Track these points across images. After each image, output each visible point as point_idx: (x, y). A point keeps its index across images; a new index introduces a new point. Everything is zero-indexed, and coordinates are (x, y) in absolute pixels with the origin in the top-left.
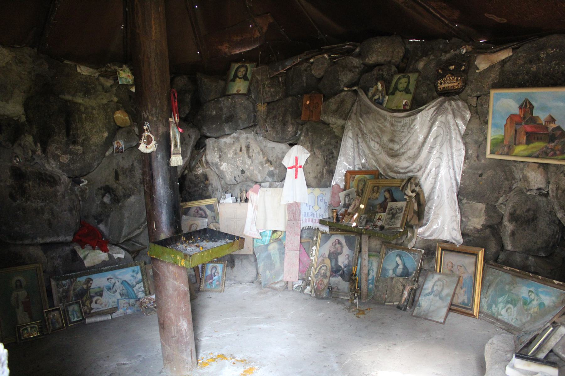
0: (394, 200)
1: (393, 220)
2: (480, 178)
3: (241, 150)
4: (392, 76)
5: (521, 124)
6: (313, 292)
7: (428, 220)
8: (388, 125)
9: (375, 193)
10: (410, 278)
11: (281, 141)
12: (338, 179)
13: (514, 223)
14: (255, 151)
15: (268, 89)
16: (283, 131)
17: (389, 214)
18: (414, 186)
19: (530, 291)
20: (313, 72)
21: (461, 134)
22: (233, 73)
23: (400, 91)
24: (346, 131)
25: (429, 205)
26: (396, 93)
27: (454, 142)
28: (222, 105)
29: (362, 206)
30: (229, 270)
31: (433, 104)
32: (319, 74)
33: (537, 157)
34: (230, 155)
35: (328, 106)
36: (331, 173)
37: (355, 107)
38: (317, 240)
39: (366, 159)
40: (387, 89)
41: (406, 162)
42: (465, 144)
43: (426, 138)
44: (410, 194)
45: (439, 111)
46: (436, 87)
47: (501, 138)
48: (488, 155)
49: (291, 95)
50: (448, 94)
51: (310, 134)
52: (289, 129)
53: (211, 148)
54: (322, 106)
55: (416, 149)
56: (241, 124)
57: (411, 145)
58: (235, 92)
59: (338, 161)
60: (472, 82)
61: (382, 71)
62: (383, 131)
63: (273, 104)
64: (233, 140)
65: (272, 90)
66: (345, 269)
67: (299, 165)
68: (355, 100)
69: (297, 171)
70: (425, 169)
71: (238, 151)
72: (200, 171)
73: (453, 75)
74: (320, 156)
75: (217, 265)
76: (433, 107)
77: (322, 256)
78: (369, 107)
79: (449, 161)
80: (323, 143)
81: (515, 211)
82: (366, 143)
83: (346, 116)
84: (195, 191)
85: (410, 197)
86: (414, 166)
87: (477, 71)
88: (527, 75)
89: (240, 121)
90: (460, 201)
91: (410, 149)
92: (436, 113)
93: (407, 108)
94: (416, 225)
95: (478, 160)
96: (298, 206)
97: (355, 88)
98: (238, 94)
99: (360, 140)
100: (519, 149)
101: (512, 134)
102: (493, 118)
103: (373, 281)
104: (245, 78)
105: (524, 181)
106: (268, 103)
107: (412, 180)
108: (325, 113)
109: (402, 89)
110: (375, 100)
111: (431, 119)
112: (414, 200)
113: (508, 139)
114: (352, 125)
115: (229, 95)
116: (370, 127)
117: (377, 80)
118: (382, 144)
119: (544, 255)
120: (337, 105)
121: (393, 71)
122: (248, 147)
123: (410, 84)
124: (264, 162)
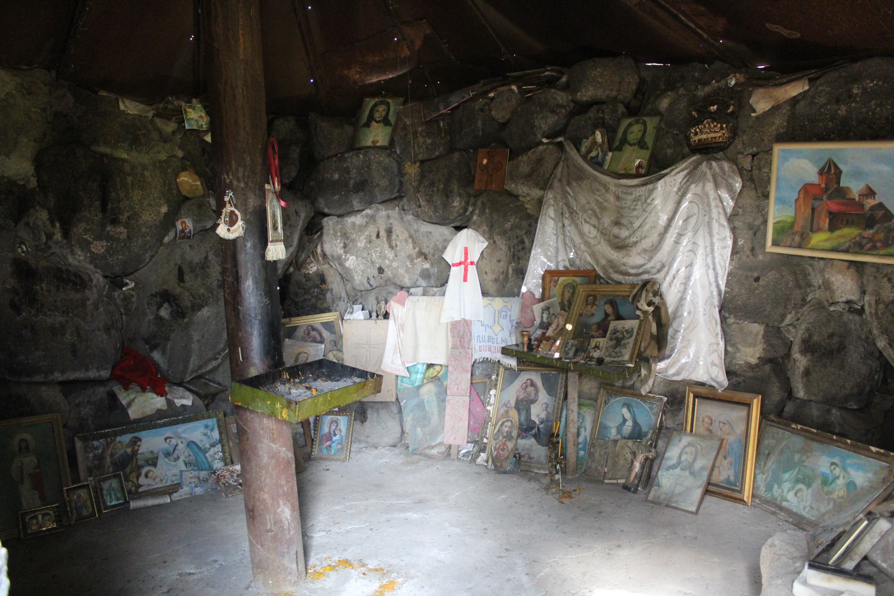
0: (619, 317)
1: (618, 349)
2: (756, 284)
3: (378, 236)
4: (619, 121)
6: (490, 463)
7: (672, 350)
8: (611, 198)
12: (532, 283)
15: (421, 140)
16: (446, 206)
17: (611, 339)
18: (651, 295)
19: (832, 464)
20: (493, 113)
22: (367, 113)
23: (631, 145)
24: (544, 207)
25: (675, 325)
27: (715, 226)
29: (569, 327)
30: (357, 425)
31: (684, 166)
32: (503, 117)
33: (846, 251)
34: (361, 244)
36: (521, 273)
38: (497, 380)
40: (611, 141)
41: (638, 257)
42: (733, 230)
43: (671, 220)
45: (692, 176)
46: (688, 138)
47: (789, 220)
48: (769, 248)
49: (460, 150)
50: (707, 150)
51: (487, 211)
52: (455, 204)
53: (332, 232)
54: (508, 166)
55: (654, 238)
56: (378, 195)
58: (369, 143)
59: (532, 255)
60: (744, 132)
61: (603, 112)
62: (603, 209)
64: (366, 220)
65: (429, 141)
66: (542, 426)
67: (469, 261)
69: (466, 270)
70: (669, 269)
71: (374, 237)
72: (313, 269)
73: (714, 120)
74: (503, 247)
75: (339, 417)
76: (682, 170)
77: (505, 405)
78: (581, 170)
80: (508, 225)
81: (810, 336)
82: (577, 226)
83: (546, 184)
84: (305, 300)
86: (651, 264)
87: (753, 115)
90: (723, 320)
91: (645, 237)
92: (688, 181)
93: (642, 171)
96: (468, 325)
97: (560, 139)
98: (375, 147)
99: (567, 222)
100: (818, 238)
101: (806, 215)
102: (778, 187)
104: (386, 121)
106: (422, 162)
107: (649, 287)
108: (512, 178)
109: (635, 141)
110: (592, 158)
111: (679, 189)
112: (651, 318)
113: (800, 223)
114: (555, 198)
115: (360, 149)
117: (596, 127)
118: (601, 228)
119: (855, 407)
121: (619, 113)
122: (389, 232)
124: (414, 256)
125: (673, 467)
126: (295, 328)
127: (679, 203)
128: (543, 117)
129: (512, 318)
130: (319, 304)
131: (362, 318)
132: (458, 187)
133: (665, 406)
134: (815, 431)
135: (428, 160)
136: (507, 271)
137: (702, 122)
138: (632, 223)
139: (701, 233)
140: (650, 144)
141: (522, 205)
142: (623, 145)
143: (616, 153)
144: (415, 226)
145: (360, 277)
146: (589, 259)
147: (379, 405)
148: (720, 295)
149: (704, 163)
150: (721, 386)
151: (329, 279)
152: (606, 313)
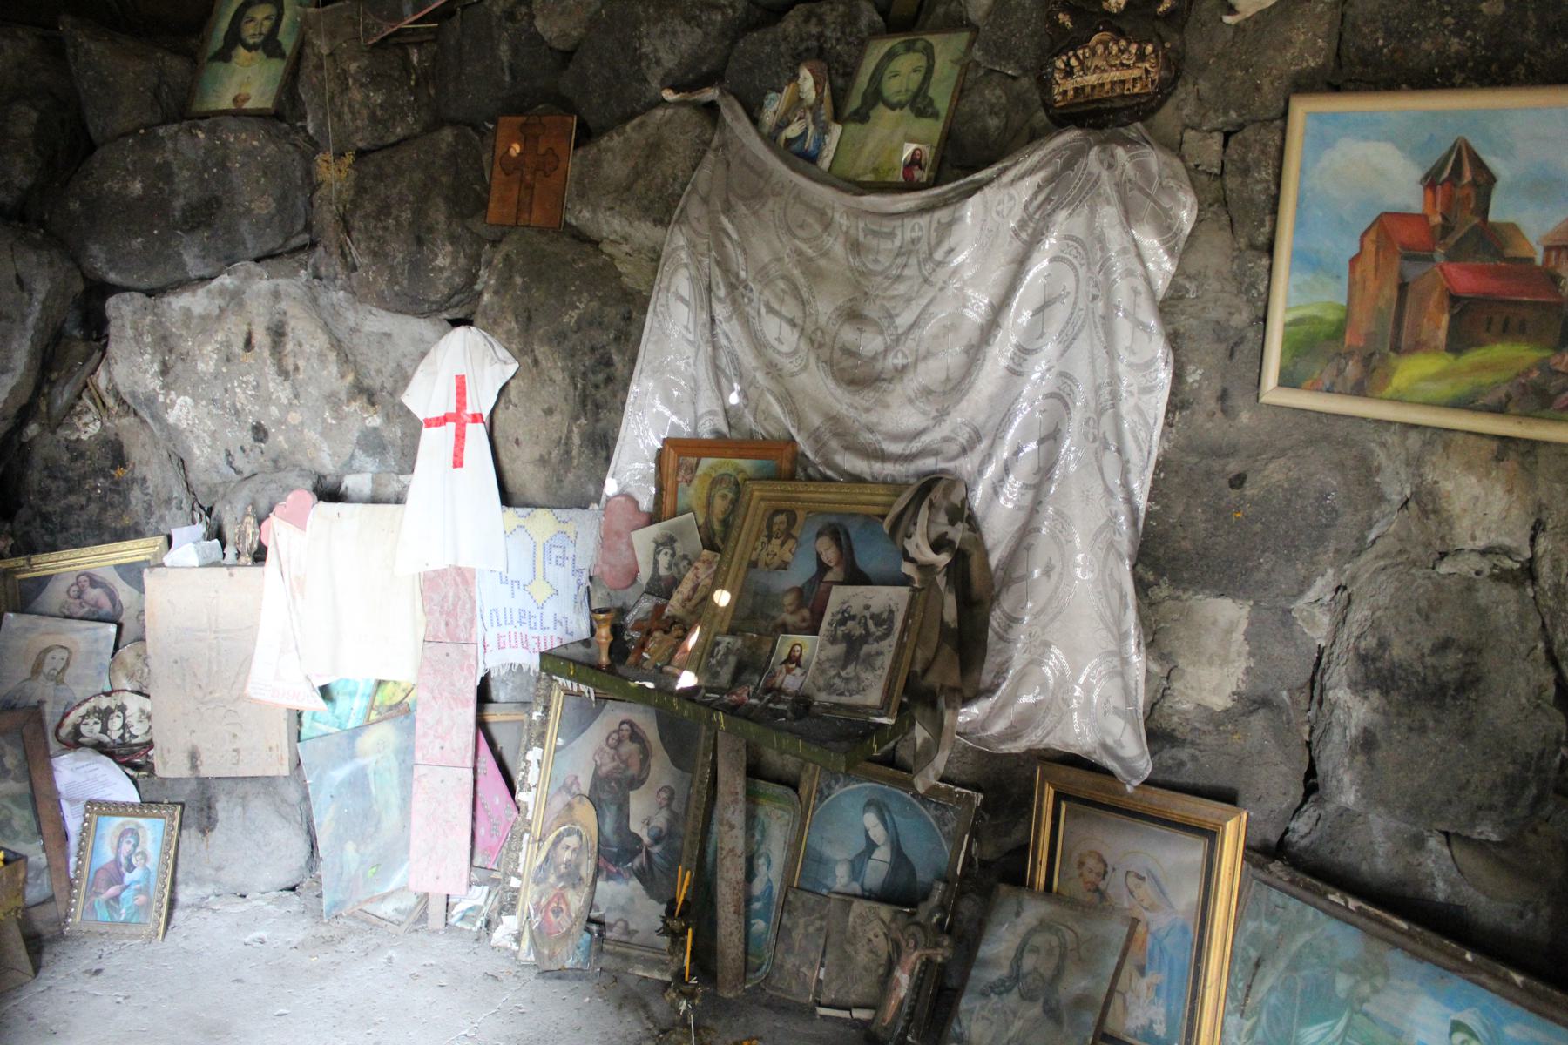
0: (856, 577)
1: (850, 669)
2: (1234, 493)
3: (248, 344)
4: (862, 44)
5: (1430, 259)
6: (525, 943)
7: (1001, 673)
8: (838, 248)
9: (776, 542)
10: (922, 912)
11: (413, 305)
12: (631, 471)
13: (1375, 696)
14: (307, 347)
15: (356, 95)
16: (418, 267)
17: (833, 640)
18: (942, 518)
19: (1457, 1026)
20: (539, 24)
21: (1152, 291)
22: (224, 25)
23: (893, 107)
24: (666, 269)
25: (1007, 602)
26: (873, 113)
27: (1123, 328)
28: (170, 157)
29: (722, 598)
30: (190, 838)
31: (1035, 158)
32: (564, 34)
33: (1499, 409)
34: (206, 365)
35: (597, 163)
36: (602, 445)
37: (703, 175)
38: (544, 722)
39: (744, 394)
40: (838, 99)
41: (909, 409)
42: (1174, 340)
43: (999, 308)
44: (928, 555)
45: (1060, 188)
46: (1045, 84)
47: (1332, 316)
48: (1271, 390)
49: (454, 123)
50: (1099, 117)
51: (518, 280)
52: (440, 262)
53: (130, 333)
54: (573, 163)
55: (951, 357)
56: (248, 238)
57: (936, 337)
58: (226, 103)
59: (631, 398)
60: (1204, 67)
61: (821, 22)
62: (815, 275)
63: (378, 156)
64: (219, 301)
65: (378, 98)
66: (656, 849)
67: (469, 411)
68: (708, 143)
69: (460, 437)
70: (992, 445)
71: (238, 348)
72: (89, 428)
73: (1120, 33)
74: (558, 377)
75: (141, 821)
76: (1031, 172)
77: (566, 788)
78: (761, 173)
79: (1100, 412)
80: (570, 318)
81: (1383, 644)
82: (746, 321)
83: (669, 210)
84: (69, 509)
85: (927, 569)
86: (945, 429)
87: (1228, 19)
88: (1460, 33)
89: (244, 227)
90: (1141, 586)
91: (929, 354)
92: (1048, 200)
93: (920, 175)
94: (955, 690)
95: (1224, 411)
96: (465, 582)
97: (711, 94)
98: (238, 114)
99: (721, 311)
100: (1412, 370)
101: (1381, 303)
102: (1300, 224)
103: (767, 906)
104: (270, 46)
105: (1425, 512)
106: (361, 154)
107: (936, 494)
108: (581, 195)
109: (903, 98)
110: (789, 142)
111: (1022, 224)
112: (941, 580)
113: (1364, 322)
114: (692, 246)
115: (205, 116)
116: (765, 256)
117: (798, 59)
118: (810, 327)
119: (1494, 838)
120: (631, 163)
121: (863, 23)
122: (278, 333)
123: (936, 75)
124: (343, 396)
125: (1001, 988)
126: (42, 582)
127: (1021, 263)
128: (664, 32)
129: (579, 565)
130: (109, 518)
131: (195, 561)
132: (449, 218)
133: (978, 816)
134: (1404, 925)
135: (380, 149)
136: (568, 438)
137: (1084, 42)
138: (891, 317)
139: (1081, 348)
140: (942, 103)
141: (610, 264)
142: (874, 105)
143: (852, 127)
144: (351, 317)
145: (207, 451)
146: (777, 410)
147: (248, 786)
148: (1134, 523)
149: (1096, 149)
150: (1133, 773)
151: (135, 453)
152: (820, 562)
